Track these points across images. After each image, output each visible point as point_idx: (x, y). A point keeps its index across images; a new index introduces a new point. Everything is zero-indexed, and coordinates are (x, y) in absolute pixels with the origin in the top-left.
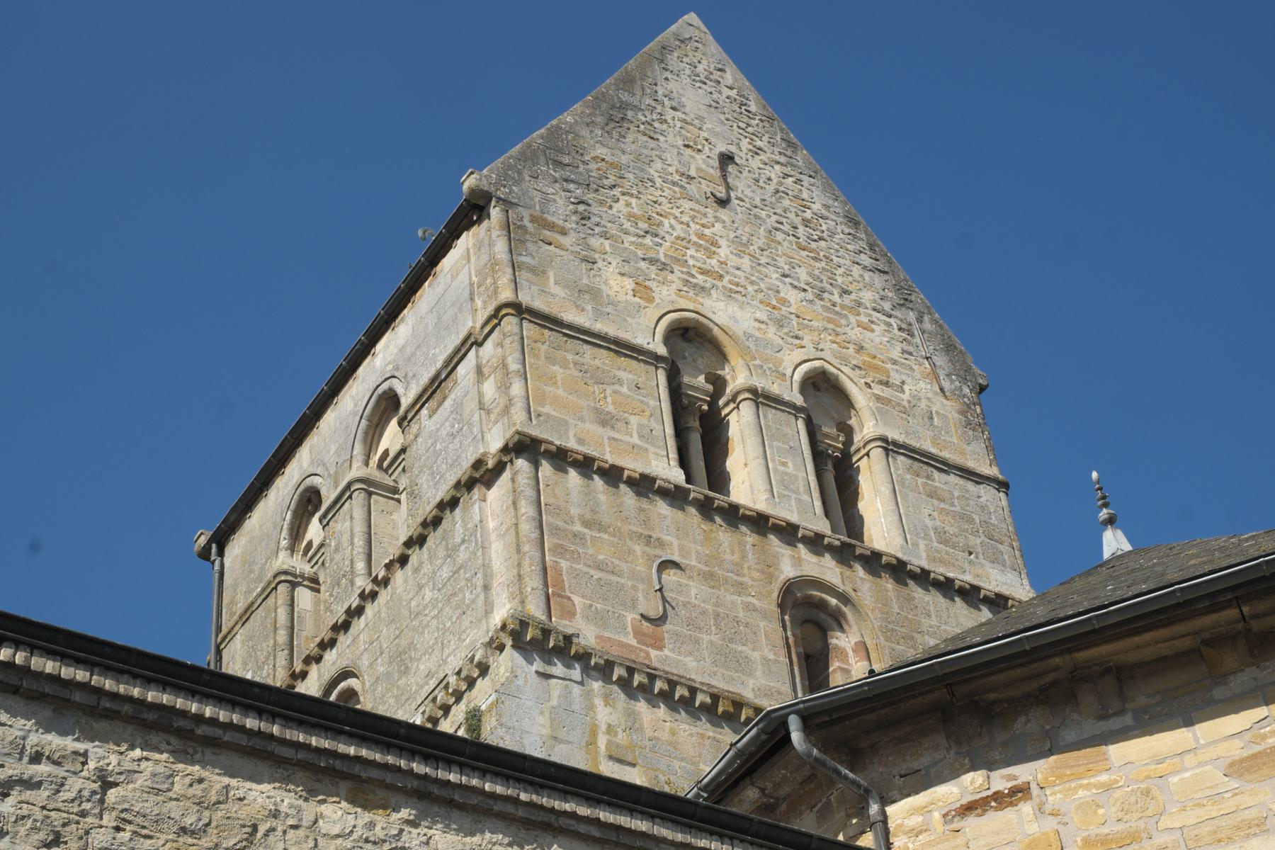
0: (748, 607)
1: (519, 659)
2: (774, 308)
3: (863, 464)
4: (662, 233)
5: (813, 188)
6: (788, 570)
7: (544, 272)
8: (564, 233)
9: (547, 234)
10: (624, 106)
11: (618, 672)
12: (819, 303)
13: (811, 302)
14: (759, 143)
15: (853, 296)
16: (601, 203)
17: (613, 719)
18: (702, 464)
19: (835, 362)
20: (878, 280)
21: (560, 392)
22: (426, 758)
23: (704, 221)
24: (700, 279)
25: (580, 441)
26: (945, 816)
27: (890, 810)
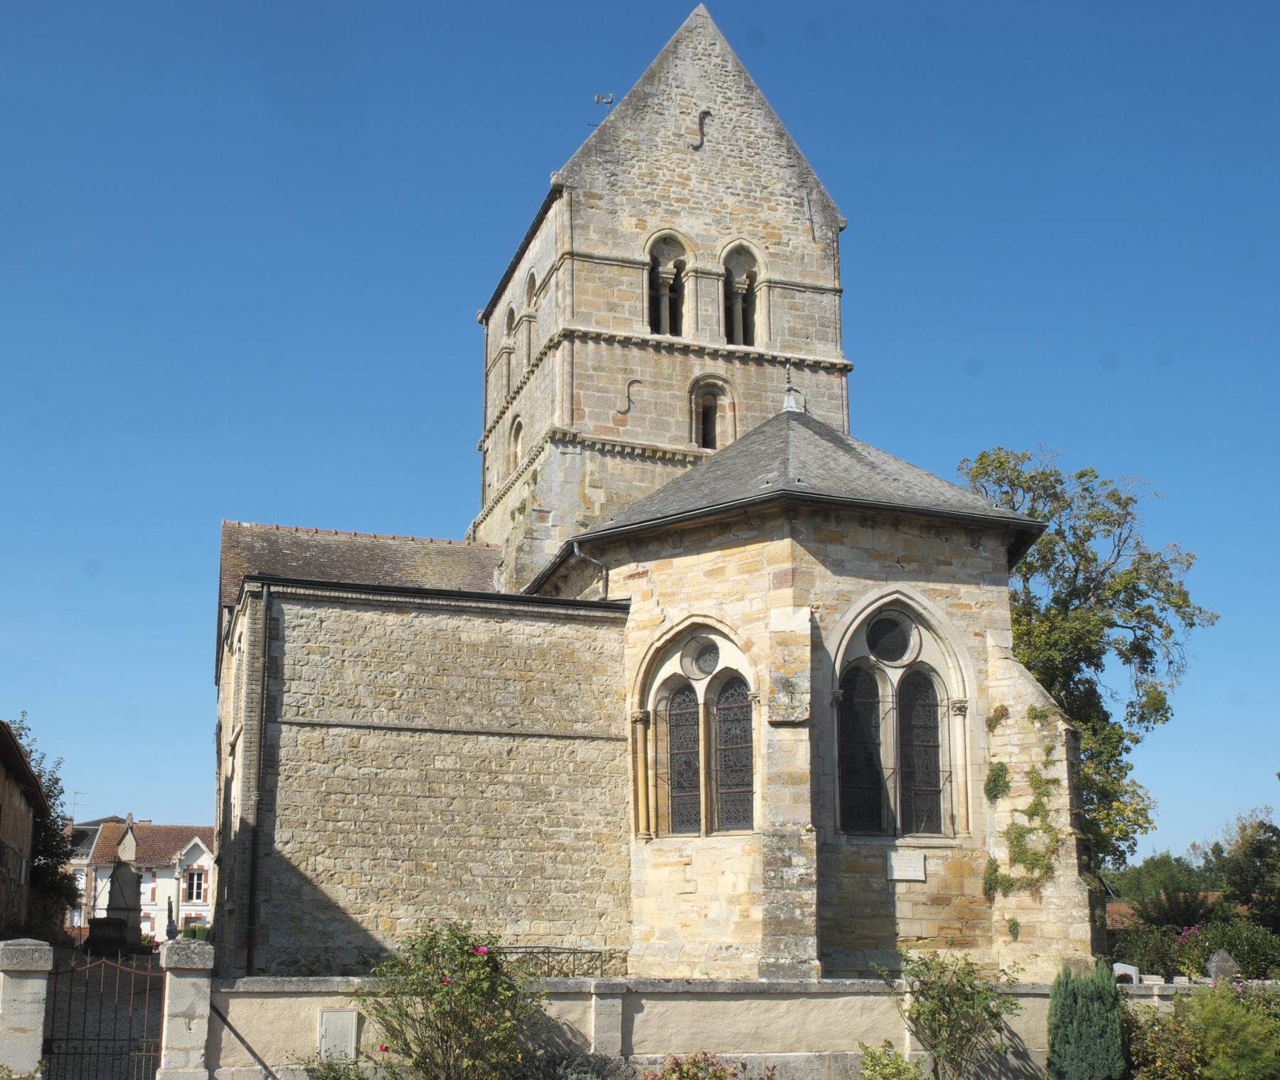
0: (673, 397)
2: (717, 212)
3: (758, 294)
4: (657, 181)
6: (697, 373)
7: (588, 227)
8: (601, 198)
11: (598, 446)
14: (729, 94)
15: (769, 190)
16: (624, 172)
17: (594, 469)
19: (749, 238)
20: (788, 173)
21: (590, 298)
22: (420, 597)
23: (684, 165)
27: (610, 572)
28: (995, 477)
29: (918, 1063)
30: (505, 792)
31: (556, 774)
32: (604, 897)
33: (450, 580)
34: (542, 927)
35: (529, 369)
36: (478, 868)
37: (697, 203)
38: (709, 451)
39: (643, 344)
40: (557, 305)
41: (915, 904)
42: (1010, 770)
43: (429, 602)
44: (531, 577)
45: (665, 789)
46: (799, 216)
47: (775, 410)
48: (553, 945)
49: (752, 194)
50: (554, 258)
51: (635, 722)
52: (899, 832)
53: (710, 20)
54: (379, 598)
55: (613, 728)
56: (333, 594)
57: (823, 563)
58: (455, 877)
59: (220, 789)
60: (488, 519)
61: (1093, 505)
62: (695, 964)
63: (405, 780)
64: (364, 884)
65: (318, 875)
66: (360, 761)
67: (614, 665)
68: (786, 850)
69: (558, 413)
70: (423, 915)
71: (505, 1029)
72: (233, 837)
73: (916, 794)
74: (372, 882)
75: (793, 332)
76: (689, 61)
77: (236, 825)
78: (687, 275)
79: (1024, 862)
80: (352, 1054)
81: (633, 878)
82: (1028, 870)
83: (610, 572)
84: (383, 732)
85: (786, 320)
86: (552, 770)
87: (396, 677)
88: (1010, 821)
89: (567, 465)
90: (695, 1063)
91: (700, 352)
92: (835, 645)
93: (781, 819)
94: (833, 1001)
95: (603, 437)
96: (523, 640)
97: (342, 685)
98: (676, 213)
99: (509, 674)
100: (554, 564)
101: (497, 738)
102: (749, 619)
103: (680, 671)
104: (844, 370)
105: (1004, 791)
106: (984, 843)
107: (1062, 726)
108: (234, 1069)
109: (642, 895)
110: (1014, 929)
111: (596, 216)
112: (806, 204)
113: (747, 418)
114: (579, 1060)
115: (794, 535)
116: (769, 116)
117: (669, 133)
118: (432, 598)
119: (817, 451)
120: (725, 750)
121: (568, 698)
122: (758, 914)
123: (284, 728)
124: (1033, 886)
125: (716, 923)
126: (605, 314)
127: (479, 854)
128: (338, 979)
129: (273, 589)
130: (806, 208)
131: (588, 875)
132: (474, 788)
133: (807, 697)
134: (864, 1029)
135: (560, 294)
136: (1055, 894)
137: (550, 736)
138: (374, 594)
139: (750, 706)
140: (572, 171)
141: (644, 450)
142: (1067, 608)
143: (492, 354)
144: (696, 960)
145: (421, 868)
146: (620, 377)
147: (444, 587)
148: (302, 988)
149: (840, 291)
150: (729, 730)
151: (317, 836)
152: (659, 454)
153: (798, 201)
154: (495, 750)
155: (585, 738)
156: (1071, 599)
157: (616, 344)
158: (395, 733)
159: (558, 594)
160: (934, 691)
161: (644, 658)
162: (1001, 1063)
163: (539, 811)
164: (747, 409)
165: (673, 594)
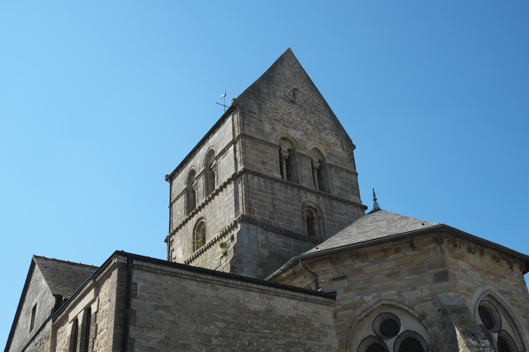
0: (295, 209)
5: (317, 97)
8: (255, 114)
9: (251, 114)
18: (286, 172)
24: (288, 124)
25: (258, 169)
26: (329, 280)
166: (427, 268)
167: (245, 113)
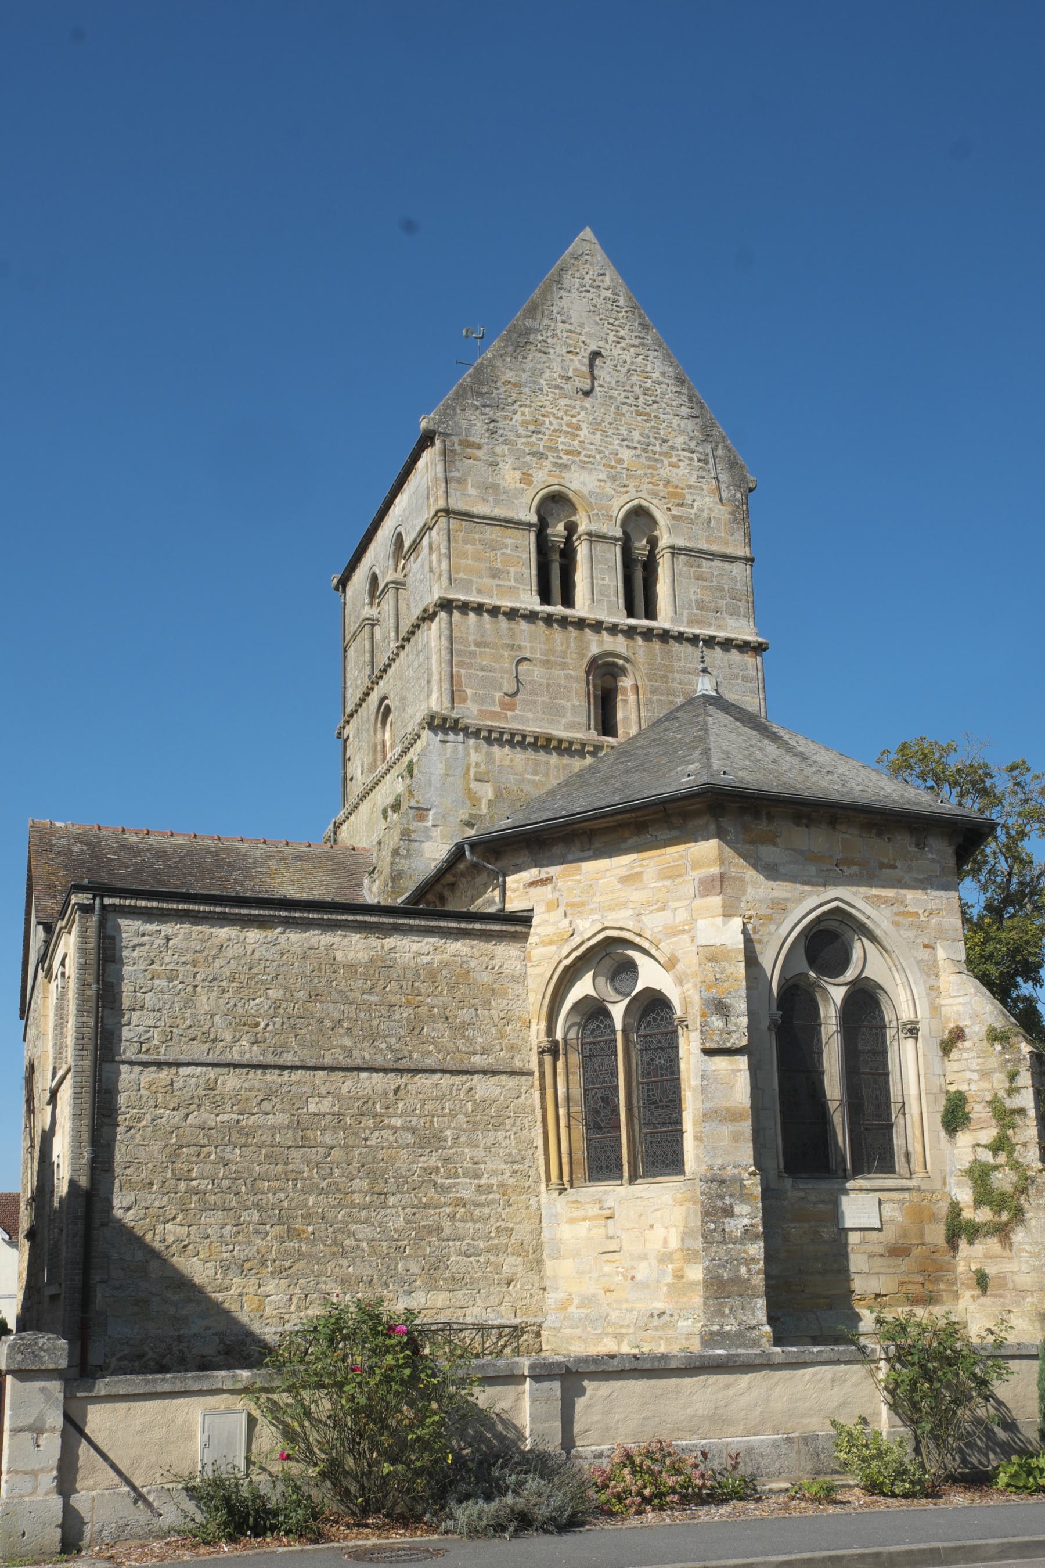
0: (568, 677)
1: (431, 734)
2: (612, 468)
3: (660, 561)
4: (543, 430)
6: (594, 650)
7: (465, 480)
8: (479, 447)
10: (529, 331)
11: (484, 734)
12: (644, 455)
13: (638, 456)
14: (622, 333)
15: (670, 444)
16: (505, 418)
17: (479, 760)
19: (648, 498)
20: (690, 425)
21: (470, 562)
22: (286, 910)
27: (508, 879)
28: (918, 770)
29: (901, 1442)
30: (392, 1138)
31: (453, 1115)
32: (512, 1260)
33: (312, 889)
34: (441, 1298)
35: (399, 644)
36: (363, 1231)
37: (589, 457)
38: (610, 739)
39: (532, 617)
40: (431, 570)
41: (871, 1256)
42: (970, 1100)
43: (297, 915)
44: (410, 886)
45: (579, 1130)
46: (704, 474)
47: (684, 694)
48: (454, 1320)
49: (650, 448)
50: (426, 515)
51: (541, 1053)
52: (849, 1172)
53: (598, 247)
54: (237, 911)
55: (516, 1060)
56: (181, 907)
57: (755, 866)
58: (335, 1243)
59: (32, 1146)
60: (352, 818)
61: (1026, 801)
62: (623, 1335)
63: (273, 1127)
64: (225, 1255)
65: (167, 1247)
66: (217, 1106)
67: (516, 986)
68: (727, 1198)
69: (435, 695)
70: (297, 1290)
71: (432, 1424)
72: (56, 1204)
73: (867, 1129)
74: (235, 1253)
75: (701, 605)
76: (575, 294)
77: (62, 1188)
78: (579, 538)
79: (989, 1203)
80: (242, 1464)
81: (546, 1235)
82: (995, 1212)
83: (508, 879)
84: (245, 1071)
85: (693, 591)
86: (447, 1111)
87: (259, 1005)
88: (972, 1158)
89: (448, 756)
90: (648, 1454)
91: (597, 626)
92: (771, 961)
93: (720, 1162)
94: (801, 1372)
95: (489, 723)
96: (409, 960)
97: (194, 1015)
98: (566, 467)
99: (394, 999)
100: (440, 870)
101: (381, 1074)
102: (673, 932)
103: (593, 993)
104: (759, 649)
105: (963, 1123)
106: (944, 1183)
107: (1025, 1048)
108: (94, 1493)
109: (557, 1256)
110: (982, 1281)
111: (474, 468)
112: (711, 460)
113: (652, 703)
114: (517, 1457)
115: (720, 835)
116: (667, 358)
117: (556, 375)
118: (300, 911)
119: (740, 739)
120: (648, 1083)
121: (464, 1026)
122: (696, 1273)
123: (124, 1068)
124: (1002, 1232)
125: (645, 1285)
126: (487, 581)
127: (364, 1213)
128: (223, 1373)
129: (107, 901)
130: (711, 466)
131: (492, 1235)
132: (356, 1134)
133: (744, 1021)
134: (835, 1404)
135: (434, 557)
136: (1027, 1240)
137: (444, 1071)
138: (231, 906)
139: (676, 1031)
140: (445, 414)
141: (536, 738)
142: (1001, 916)
143: (352, 627)
144: (624, 1331)
145: (294, 1234)
146: (506, 654)
147: (305, 896)
148: (179, 1387)
149: (752, 560)
150: (652, 1060)
151: (166, 1199)
152: (553, 744)
153: (702, 457)
154: (379, 1089)
155: (484, 1072)
156: (1005, 907)
157: (500, 616)
158: (259, 1072)
159: (443, 905)
160: (881, 1011)
161: (551, 978)
162: (988, 1438)
163: (434, 1160)
164: (652, 692)
165: (583, 904)
166: (689, 868)
167: (453, 451)
